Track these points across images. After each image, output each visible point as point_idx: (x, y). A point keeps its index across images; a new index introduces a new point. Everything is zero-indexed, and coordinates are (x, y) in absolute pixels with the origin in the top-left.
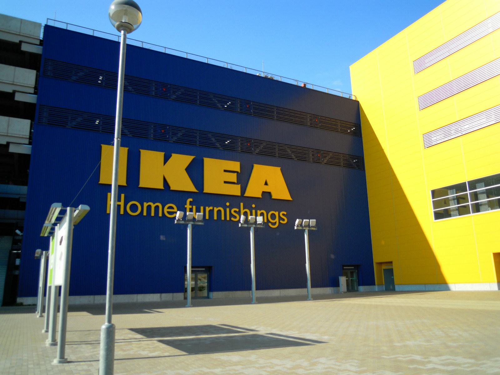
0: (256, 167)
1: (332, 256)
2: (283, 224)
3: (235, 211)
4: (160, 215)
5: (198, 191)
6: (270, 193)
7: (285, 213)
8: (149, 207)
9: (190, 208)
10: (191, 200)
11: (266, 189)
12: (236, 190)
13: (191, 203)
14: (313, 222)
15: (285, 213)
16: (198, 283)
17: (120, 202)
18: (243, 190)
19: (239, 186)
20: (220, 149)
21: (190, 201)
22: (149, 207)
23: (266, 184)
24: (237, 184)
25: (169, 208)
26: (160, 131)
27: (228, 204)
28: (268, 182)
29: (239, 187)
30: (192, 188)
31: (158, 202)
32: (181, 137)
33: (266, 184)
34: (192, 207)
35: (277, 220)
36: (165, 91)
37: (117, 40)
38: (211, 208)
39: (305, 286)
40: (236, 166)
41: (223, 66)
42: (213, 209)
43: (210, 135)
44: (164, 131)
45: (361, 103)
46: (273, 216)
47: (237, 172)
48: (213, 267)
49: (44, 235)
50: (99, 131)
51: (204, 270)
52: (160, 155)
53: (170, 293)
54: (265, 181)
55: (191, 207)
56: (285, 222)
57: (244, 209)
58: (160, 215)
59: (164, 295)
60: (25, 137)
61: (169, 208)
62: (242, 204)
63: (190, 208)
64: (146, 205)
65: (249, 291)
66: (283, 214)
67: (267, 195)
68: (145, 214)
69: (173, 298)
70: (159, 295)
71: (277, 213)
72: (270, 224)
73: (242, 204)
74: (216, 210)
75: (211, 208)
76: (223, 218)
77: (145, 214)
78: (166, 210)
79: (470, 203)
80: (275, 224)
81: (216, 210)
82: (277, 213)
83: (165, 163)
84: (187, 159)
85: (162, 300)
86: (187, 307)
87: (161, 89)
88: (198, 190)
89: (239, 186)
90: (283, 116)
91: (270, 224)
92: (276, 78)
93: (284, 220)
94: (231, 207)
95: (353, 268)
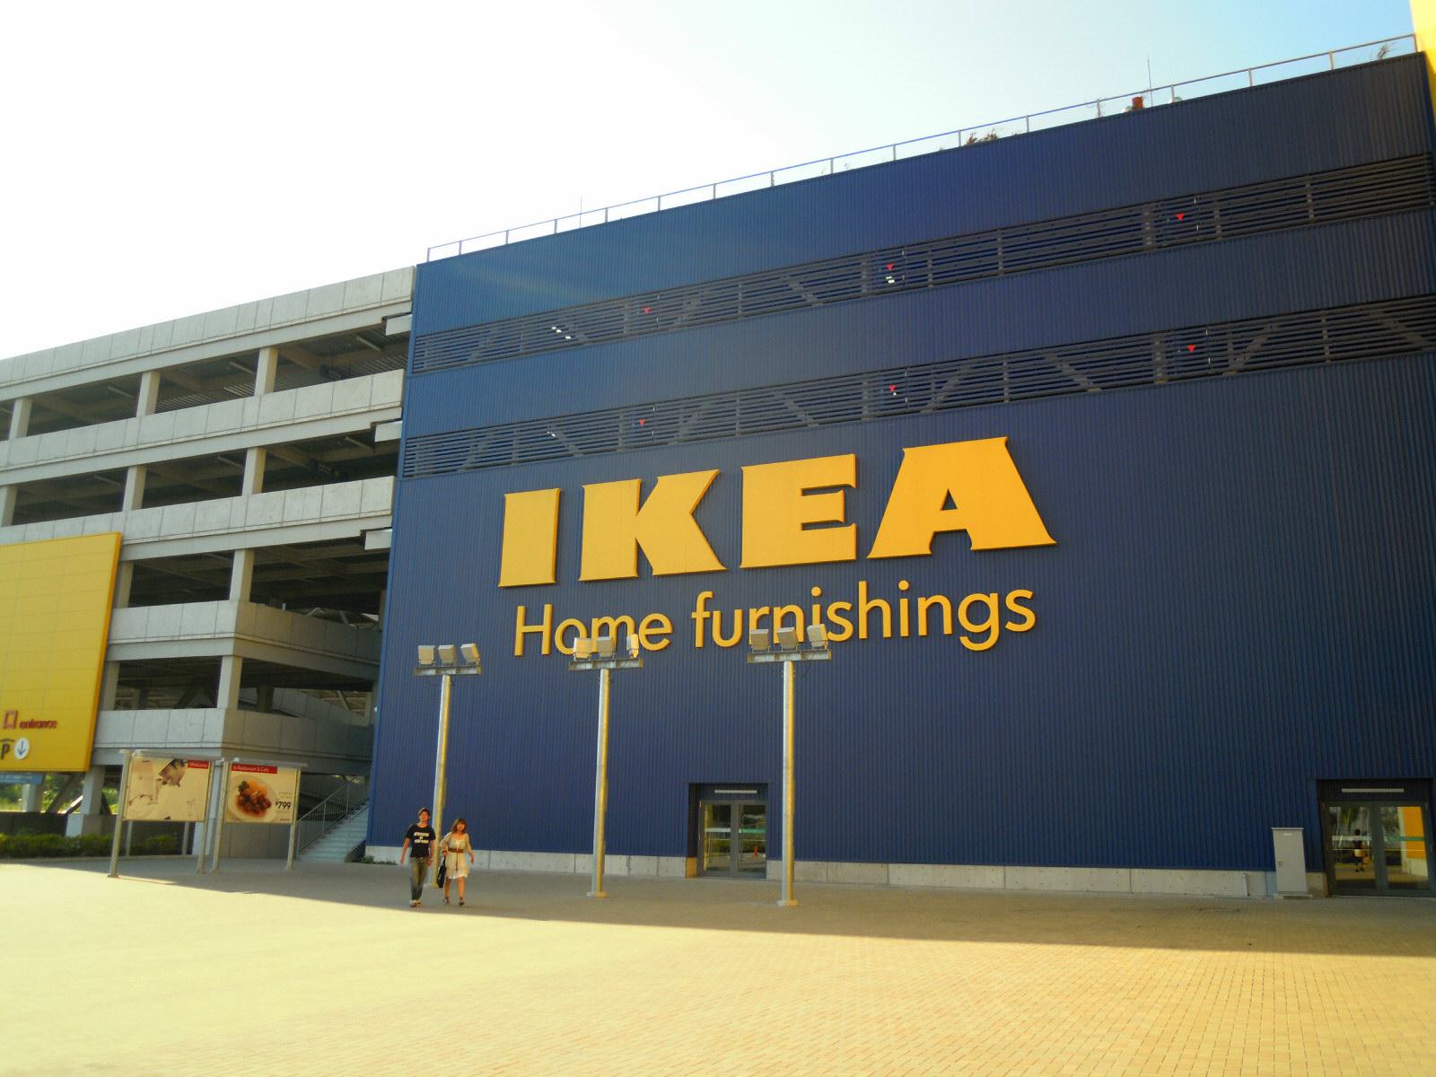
0: (513, 500)
2: (736, 645)
3: (839, 612)
5: (724, 568)
6: (963, 533)
7: (1028, 594)
9: (705, 619)
10: (709, 594)
11: (949, 522)
12: (840, 545)
13: (708, 604)
15: (1028, 594)
17: (542, 624)
18: (865, 540)
19: (851, 530)
20: (1090, 390)
21: (706, 600)
23: (949, 503)
24: (846, 523)
25: (650, 626)
26: (636, 424)
27: (816, 591)
30: (709, 562)
31: (881, 598)
32: (1265, 348)
33: (949, 503)
34: (712, 615)
35: (993, 621)
36: (650, 314)
37: (1410, 51)
38: (765, 610)
39: (587, 848)
40: (841, 469)
41: (577, 227)
42: (771, 611)
43: (1050, 358)
44: (1194, 346)
46: (977, 612)
47: (845, 487)
48: (769, 787)
50: (1324, 361)
51: (754, 795)
52: (628, 489)
53: (569, 852)
54: (946, 492)
55: (707, 614)
57: (868, 601)
59: (637, 860)
60: (384, 513)
61: (650, 626)
62: (862, 586)
63: (705, 619)
65: (885, 865)
66: (1018, 600)
67: (950, 543)
69: (658, 870)
70: (624, 858)
71: (992, 601)
72: (965, 641)
73: (862, 586)
75: (765, 610)
76: (887, 633)
82: (992, 601)
84: (693, 485)
85: (632, 872)
87: (643, 311)
88: (1054, 539)
89: (851, 530)
90: (1285, 208)
91: (965, 641)
92: (1005, 132)
94: (824, 601)
95: (1402, 790)
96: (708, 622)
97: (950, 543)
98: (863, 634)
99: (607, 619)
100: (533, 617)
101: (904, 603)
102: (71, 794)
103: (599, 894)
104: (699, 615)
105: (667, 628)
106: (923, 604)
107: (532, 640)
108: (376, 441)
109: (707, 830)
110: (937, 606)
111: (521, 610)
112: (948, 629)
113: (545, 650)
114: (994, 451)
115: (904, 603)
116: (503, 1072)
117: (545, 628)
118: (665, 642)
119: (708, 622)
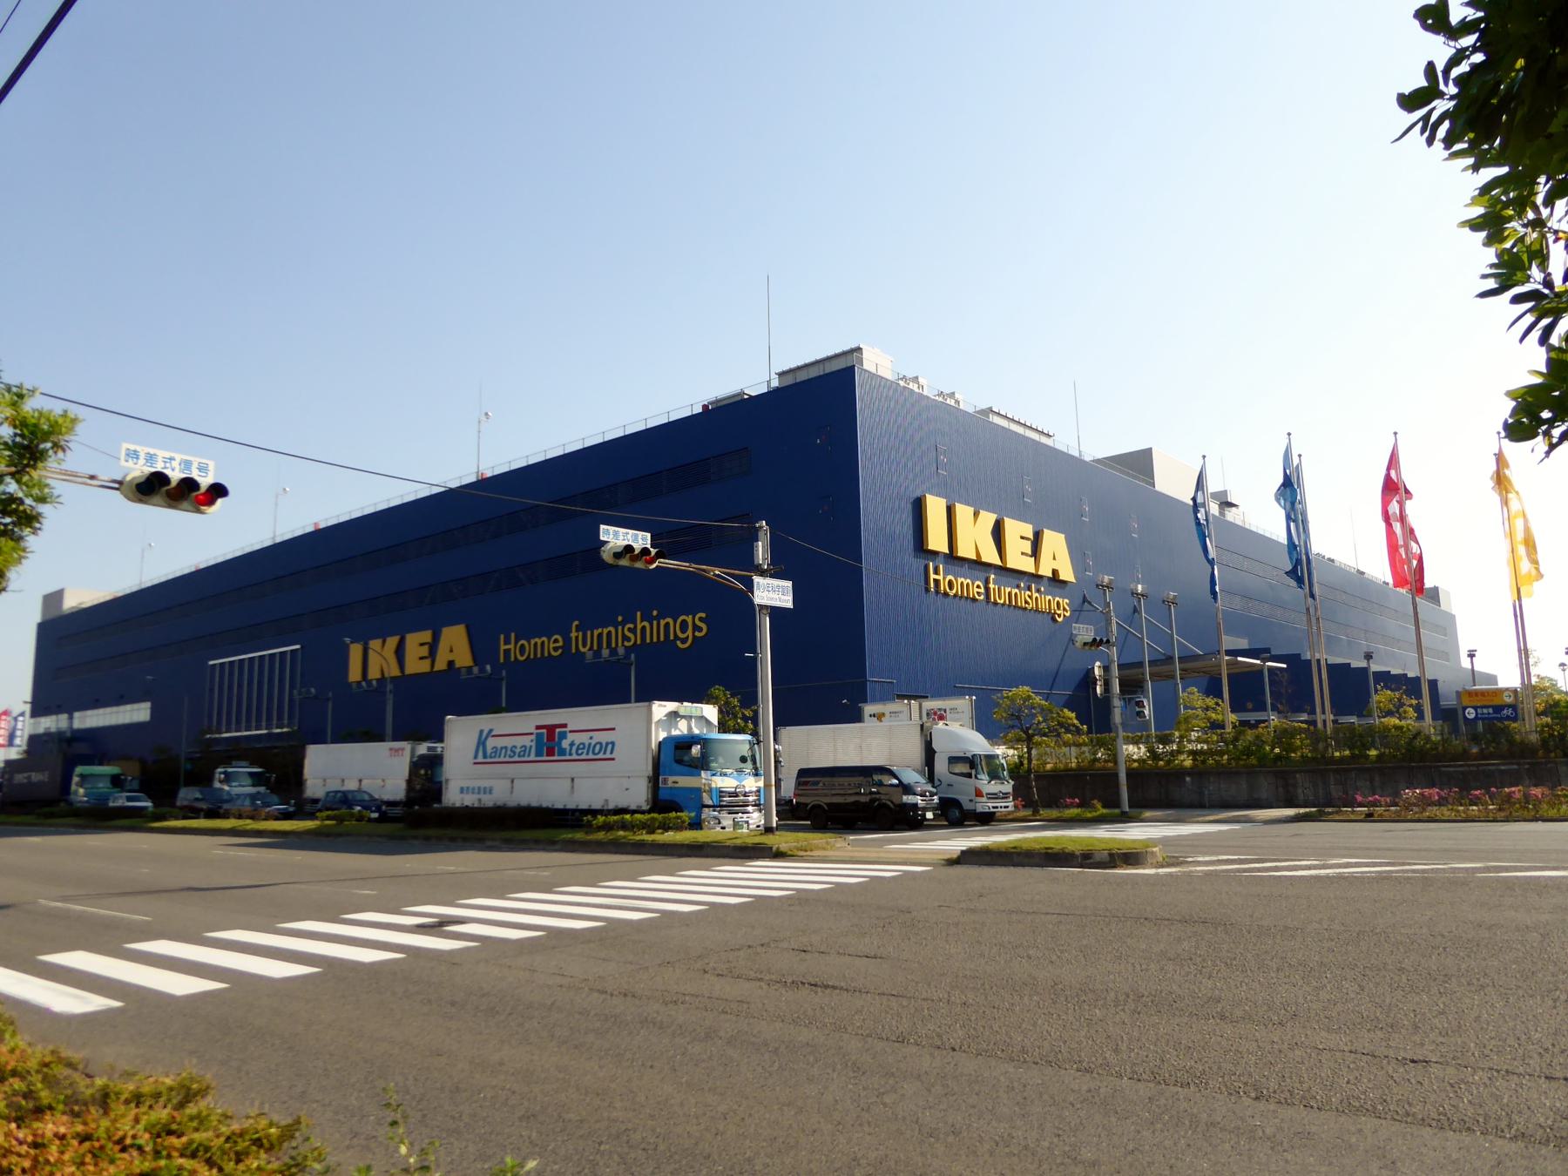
1: (1430, 21)
7: (703, 615)
10: (576, 623)
15: (703, 615)
21: (577, 626)
23: (451, 651)
28: (454, 649)
33: (451, 651)
35: (690, 632)
57: (642, 621)
72: (678, 642)
74: (605, 631)
75: (600, 630)
78: (552, 645)
80: (684, 641)
81: (605, 631)
82: (689, 619)
86: (181, 510)
93: (700, 630)
94: (623, 623)
96: (577, 638)
98: (639, 642)
99: (537, 640)
101: (655, 623)
102: (1001, 735)
103: (1154, 849)
104: (573, 635)
106: (663, 623)
108: (1426, 84)
110: (610, 632)
111: (639, 614)
112: (672, 638)
113: (512, 659)
115: (655, 623)
117: (511, 646)
118: (560, 651)
119: (577, 638)
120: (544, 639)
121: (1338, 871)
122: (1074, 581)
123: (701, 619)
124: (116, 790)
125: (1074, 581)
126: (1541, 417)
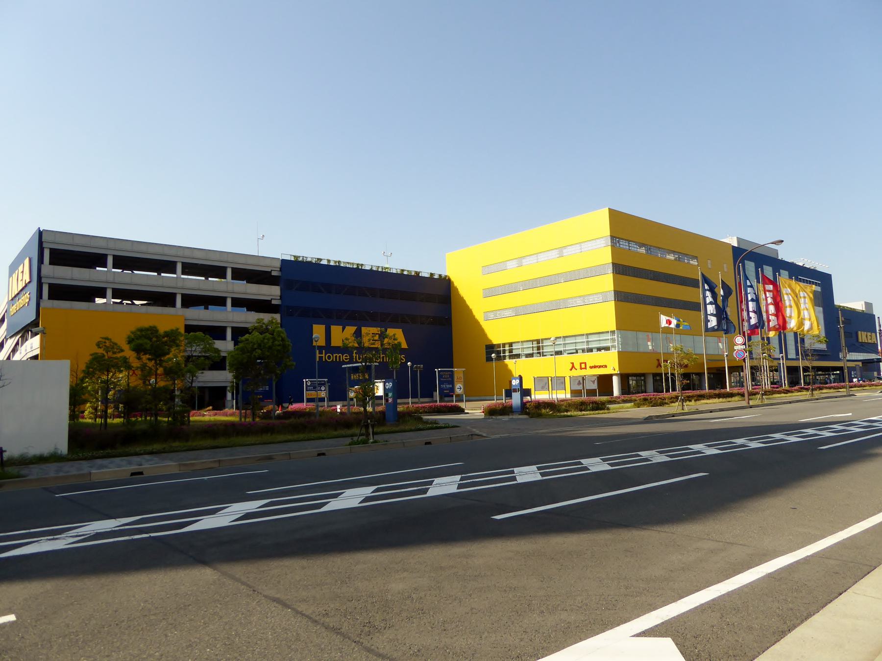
4: (342, 360)
8: (336, 356)
12: (709, 313)
13: (356, 353)
14: (422, 366)
16: (288, 603)
18: (709, 315)
22: (336, 356)
29: (524, 401)
45: (452, 279)
49: (496, 315)
56: (404, 361)
58: (342, 360)
64: (334, 355)
68: (334, 360)
77: (334, 360)
78: (344, 358)
79: (502, 349)
81: (338, 356)
83: (343, 331)
84: (353, 329)
93: (403, 360)
96: (356, 357)
97: (709, 321)
99: (337, 354)
100: (321, 353)
104: (354, 355)
105: (348, 357)
107: (321, 358)
109: (728, 390)
114: (400, 330)
116: (270, 458)
117: (324, 355)
119: (356, 357)
120: (340, 355)
121: (794, 395)
122: (356, 327)
123: (403, 357)
124: (811, 296)
125: (356, 327)
126: (822, 289)
